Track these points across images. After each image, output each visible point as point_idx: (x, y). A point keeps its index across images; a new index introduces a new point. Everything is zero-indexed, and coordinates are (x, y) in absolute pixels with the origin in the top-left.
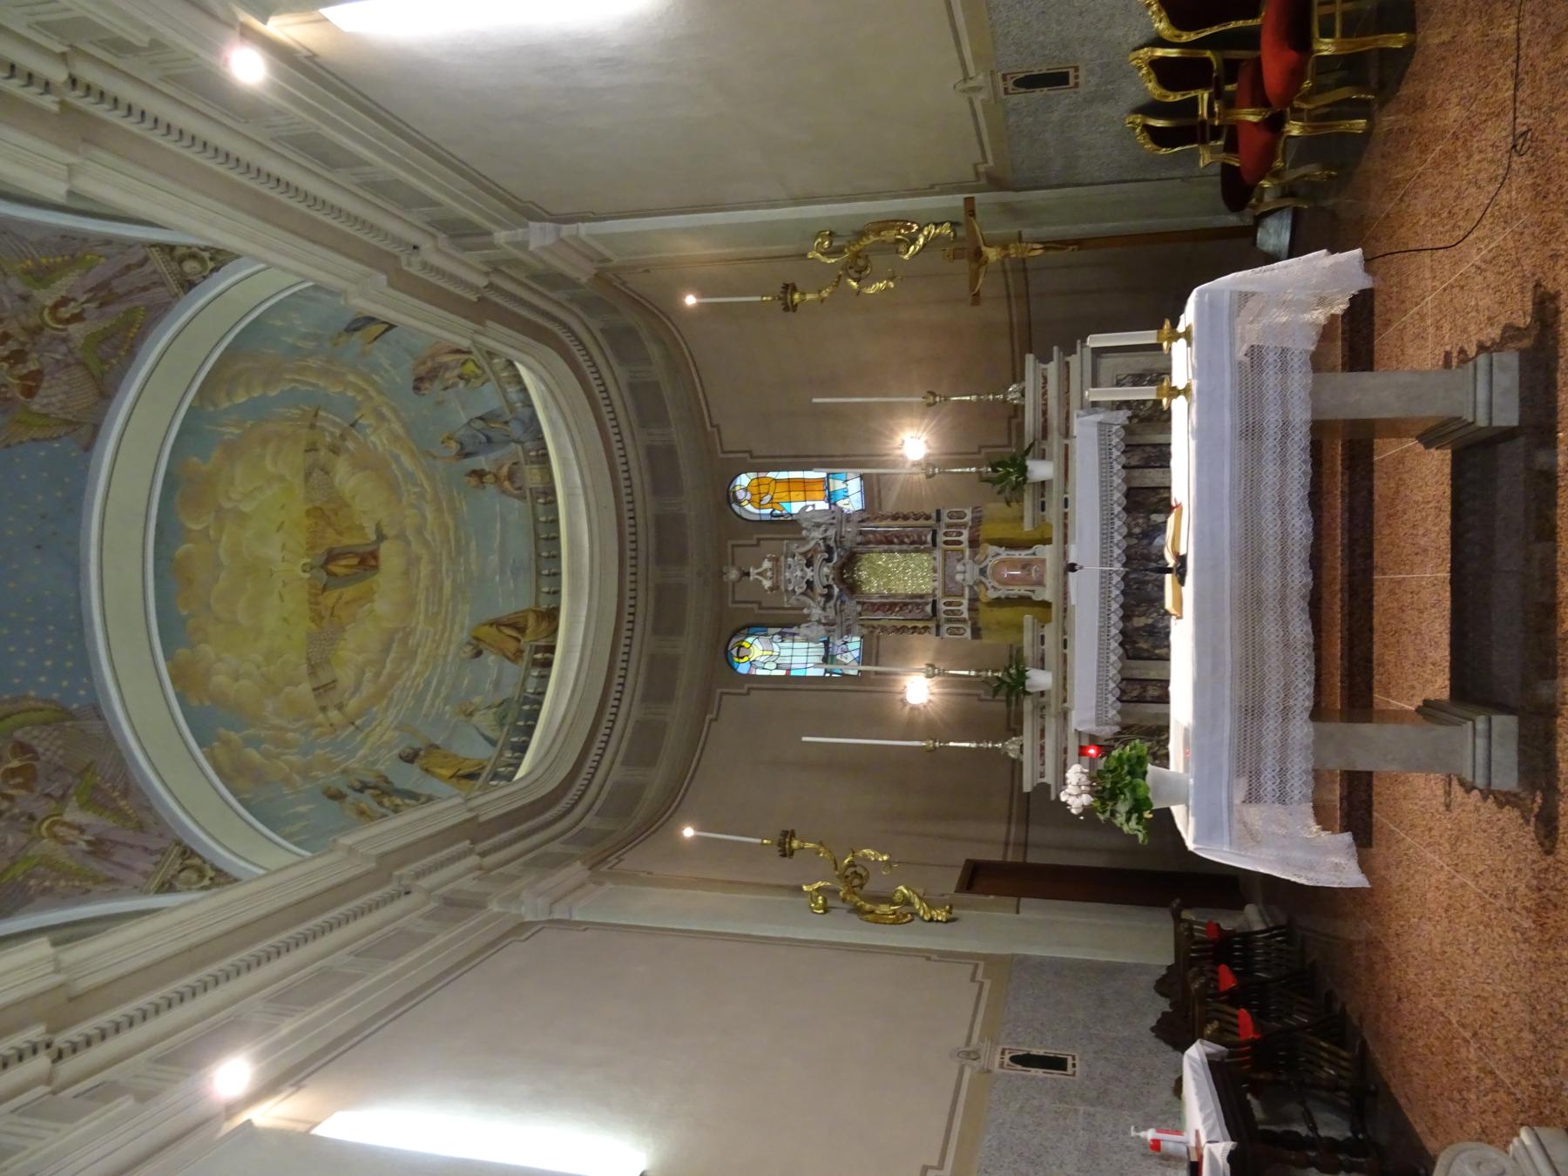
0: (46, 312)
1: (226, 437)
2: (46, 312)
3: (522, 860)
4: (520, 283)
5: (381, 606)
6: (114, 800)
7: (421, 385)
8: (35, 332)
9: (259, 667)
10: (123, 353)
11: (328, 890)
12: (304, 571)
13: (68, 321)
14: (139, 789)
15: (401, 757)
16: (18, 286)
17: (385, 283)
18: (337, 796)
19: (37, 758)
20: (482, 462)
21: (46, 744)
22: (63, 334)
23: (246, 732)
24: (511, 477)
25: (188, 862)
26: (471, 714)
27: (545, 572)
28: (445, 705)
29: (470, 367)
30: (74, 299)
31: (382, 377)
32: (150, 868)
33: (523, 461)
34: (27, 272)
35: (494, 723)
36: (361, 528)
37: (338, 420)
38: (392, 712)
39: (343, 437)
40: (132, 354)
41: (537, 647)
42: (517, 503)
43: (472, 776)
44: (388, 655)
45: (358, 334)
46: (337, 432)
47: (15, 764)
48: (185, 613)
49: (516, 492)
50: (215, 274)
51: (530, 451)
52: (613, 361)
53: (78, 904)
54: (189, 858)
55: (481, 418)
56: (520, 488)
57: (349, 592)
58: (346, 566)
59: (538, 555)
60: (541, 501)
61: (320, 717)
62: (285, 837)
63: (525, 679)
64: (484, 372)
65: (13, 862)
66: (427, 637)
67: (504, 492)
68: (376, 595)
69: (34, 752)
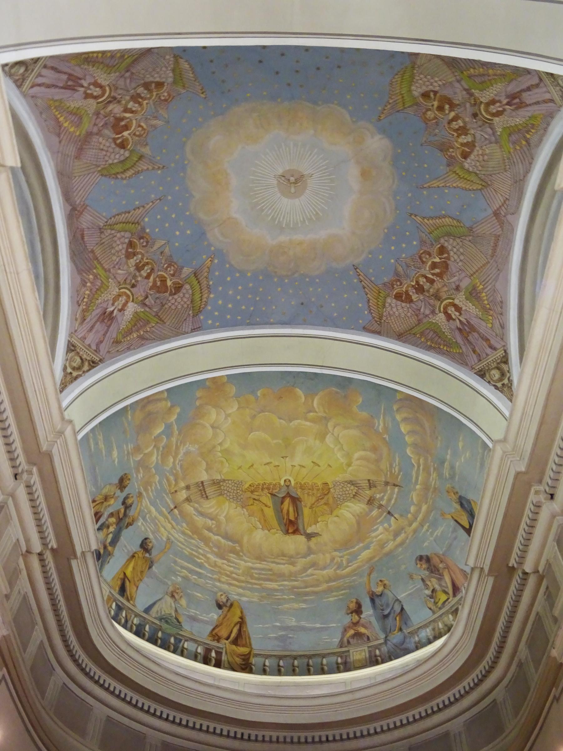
0: (482, 107)
1: (376, 421)
2: (482, 107)
3: (31, 595)
4: (532, 605)
5: (259, 535)
6: (138, 331)
7: (424, 561)
8: (437, 297)
9: (220, 444)
10: (429, 343)
11: (32, 421)
12: (285, 481)
13: (446, 313)
14: (142, 345)
15: (146, 539)
16: (465, 284)
17: (519, 470)
18: (122, 483)
19: (171, 294)
20: (368, 612)
21: (179, 300)
22: (437, 311)
23: (175, 427)
24: (358, 635)
25: (86, 364)
26: (173, 596)
27: (281, 663)
28: (182, 577)
29: (443, 597)
30: (461, 314)
31: (427, 530)
32: (87, 342)
33: (371, 644)
34: (474, 288)
35: (163, 613)
36: (316, 522)
37: (393, 502)
38: (181, 538)
39: (380, 506)
40: (429, 348)
41: (221, 653)
42: (336, 640)
43: (123, 590)
44: (223, 538)
45: (458, 507)
46: (383, 503)
47: (169, 283)
48: (259, 393)
49: (345, 640)
50: (493, 388)
51: (379, 650)
52: (468, 715)
53: (71, 297)
54: (89, 364)
55: (402, 609)
56: (349, 642)
57: (270, 512)
58: (288, 511)
59: (295, 658)
60: (340, 660)
61: (182, 484)
62: (92, 430)
63: (195, 641)
64: (440, 609)
65: (107, 271)
66: (234, 568)
67: (345, 630)
68: (266, 531)
69: (175, 294)
